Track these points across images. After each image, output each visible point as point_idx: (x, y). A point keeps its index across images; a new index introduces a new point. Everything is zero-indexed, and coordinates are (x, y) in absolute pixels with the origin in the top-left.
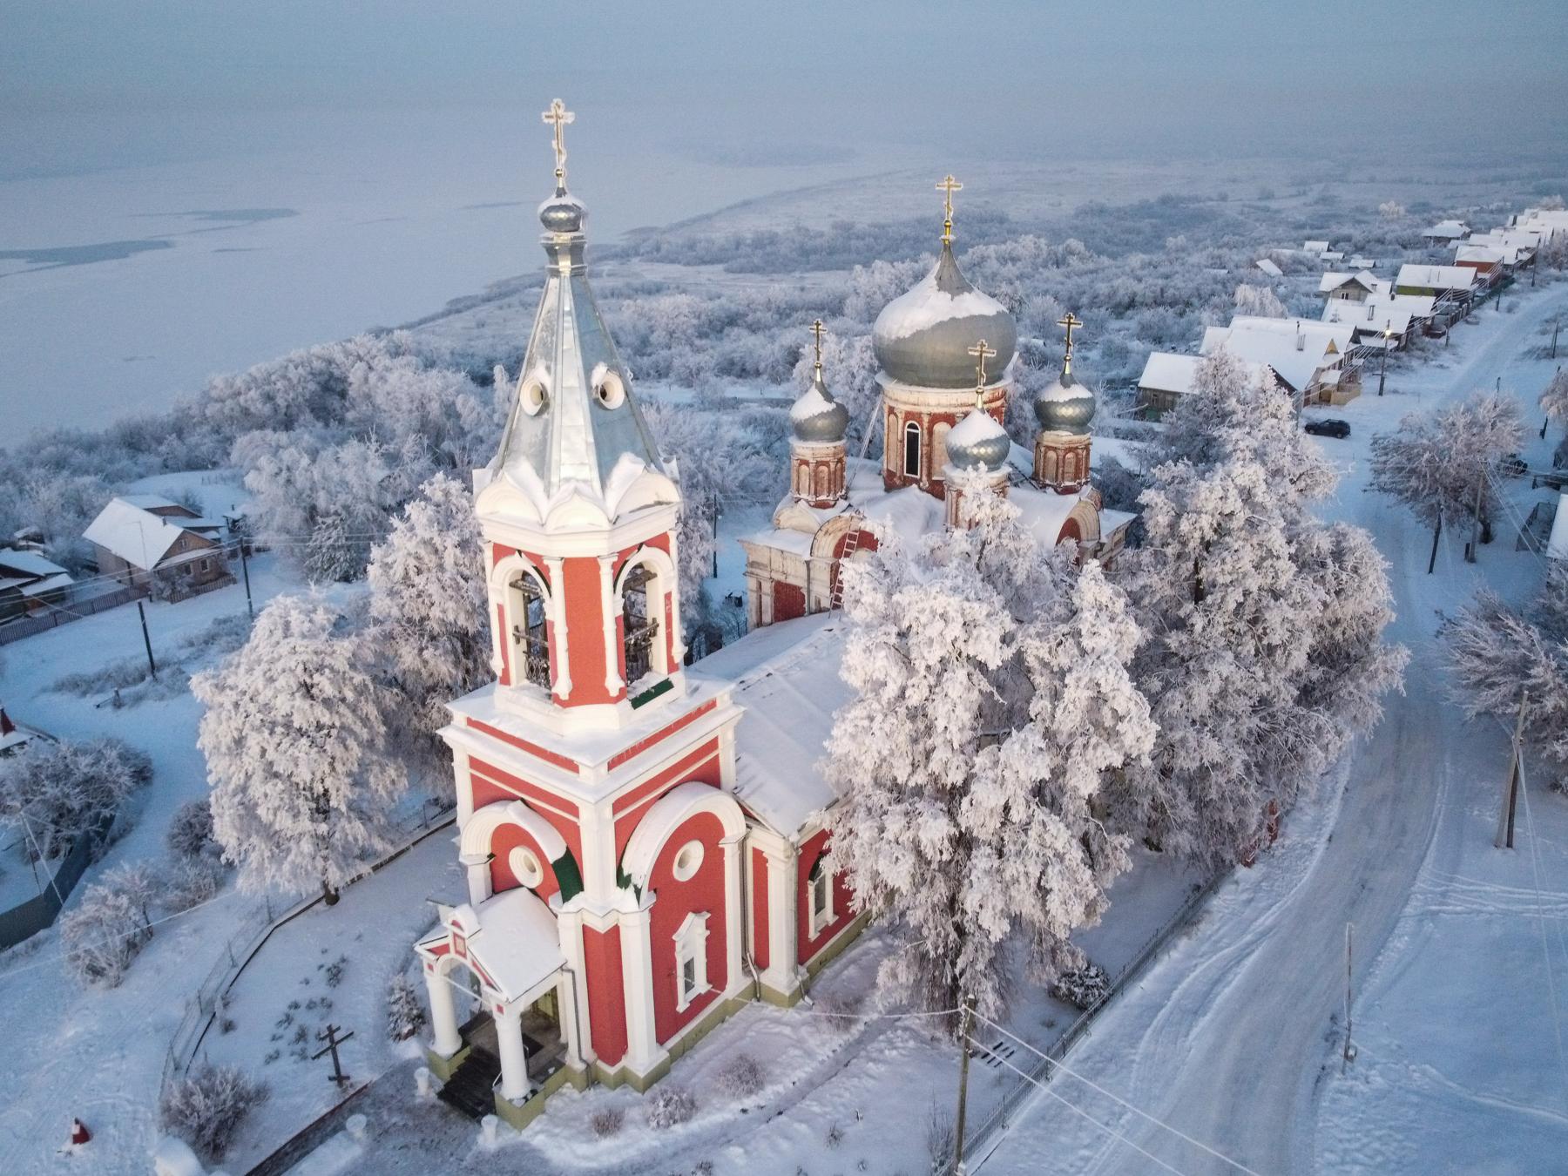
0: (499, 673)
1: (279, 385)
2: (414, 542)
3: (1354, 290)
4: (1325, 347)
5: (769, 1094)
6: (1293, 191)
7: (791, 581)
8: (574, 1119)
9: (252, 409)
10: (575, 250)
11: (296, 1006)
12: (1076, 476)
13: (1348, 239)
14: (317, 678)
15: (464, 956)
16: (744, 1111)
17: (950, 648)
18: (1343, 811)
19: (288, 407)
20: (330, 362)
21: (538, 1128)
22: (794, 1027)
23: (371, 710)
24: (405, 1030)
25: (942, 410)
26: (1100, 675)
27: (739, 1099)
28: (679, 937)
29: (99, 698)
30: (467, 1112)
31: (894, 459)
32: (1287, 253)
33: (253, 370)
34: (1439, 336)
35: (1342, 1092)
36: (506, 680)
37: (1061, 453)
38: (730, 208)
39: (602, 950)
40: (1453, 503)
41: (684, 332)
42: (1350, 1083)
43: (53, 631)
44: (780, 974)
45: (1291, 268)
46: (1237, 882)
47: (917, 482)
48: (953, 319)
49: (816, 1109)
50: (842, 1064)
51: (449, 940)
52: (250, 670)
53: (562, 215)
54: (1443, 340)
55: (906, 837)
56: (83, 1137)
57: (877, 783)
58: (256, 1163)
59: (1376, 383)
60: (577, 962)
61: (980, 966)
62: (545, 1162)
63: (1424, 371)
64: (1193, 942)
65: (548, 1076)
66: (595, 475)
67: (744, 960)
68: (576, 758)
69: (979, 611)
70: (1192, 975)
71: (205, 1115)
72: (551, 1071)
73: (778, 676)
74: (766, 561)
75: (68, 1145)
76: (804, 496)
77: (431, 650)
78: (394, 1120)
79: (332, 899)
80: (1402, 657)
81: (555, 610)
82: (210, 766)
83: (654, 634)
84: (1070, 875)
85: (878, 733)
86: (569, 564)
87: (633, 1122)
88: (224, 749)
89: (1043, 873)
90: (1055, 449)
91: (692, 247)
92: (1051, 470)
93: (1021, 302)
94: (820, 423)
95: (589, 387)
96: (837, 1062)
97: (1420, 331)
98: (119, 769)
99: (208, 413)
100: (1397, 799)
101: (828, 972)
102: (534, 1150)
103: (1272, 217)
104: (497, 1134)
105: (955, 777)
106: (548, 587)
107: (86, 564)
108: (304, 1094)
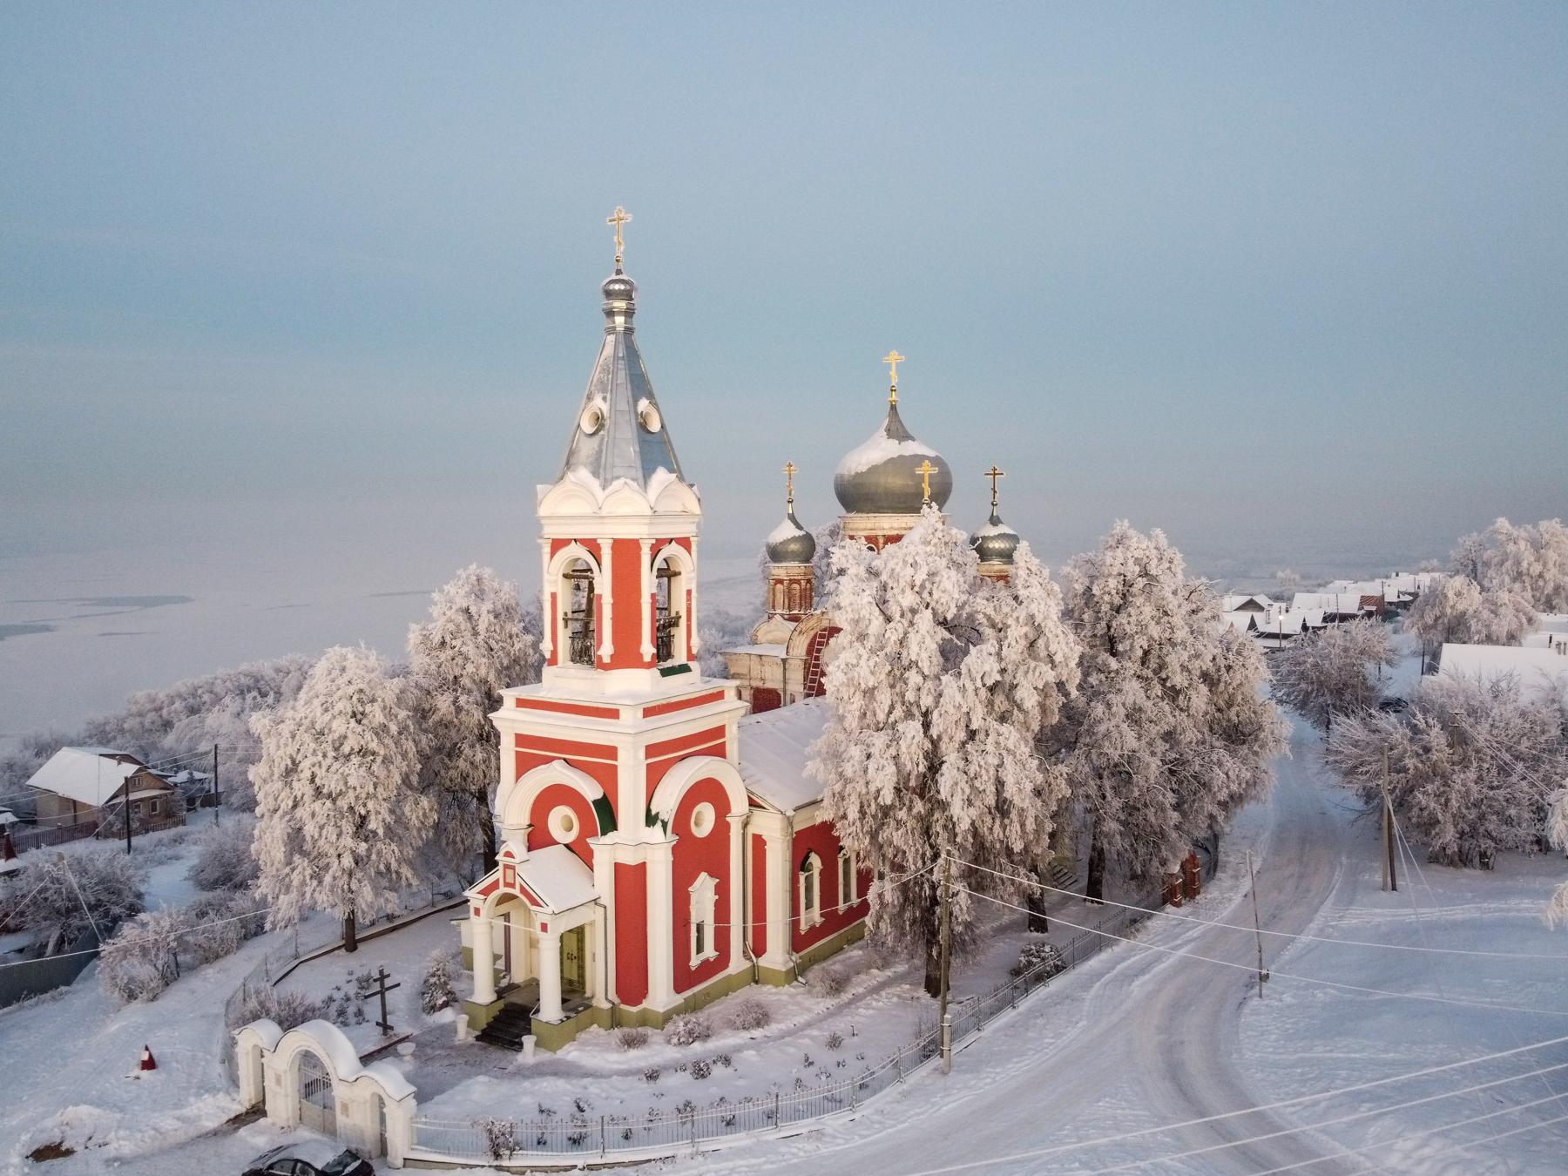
0: (548, 655)
5: (773, 1029)
7: (769, 685)
10: (629, 313)
14: (368, 708)
23: (409, 746)
25: (894, 533)
39: (630, 881)
44: (777, 955)
48: (901, 457)
50: (830, 1014)
56: (150, 1064)
74: (745, 671)
75: (137, 1072)
81: (604, 584)
86: (618, 545)
94: (793, 547)
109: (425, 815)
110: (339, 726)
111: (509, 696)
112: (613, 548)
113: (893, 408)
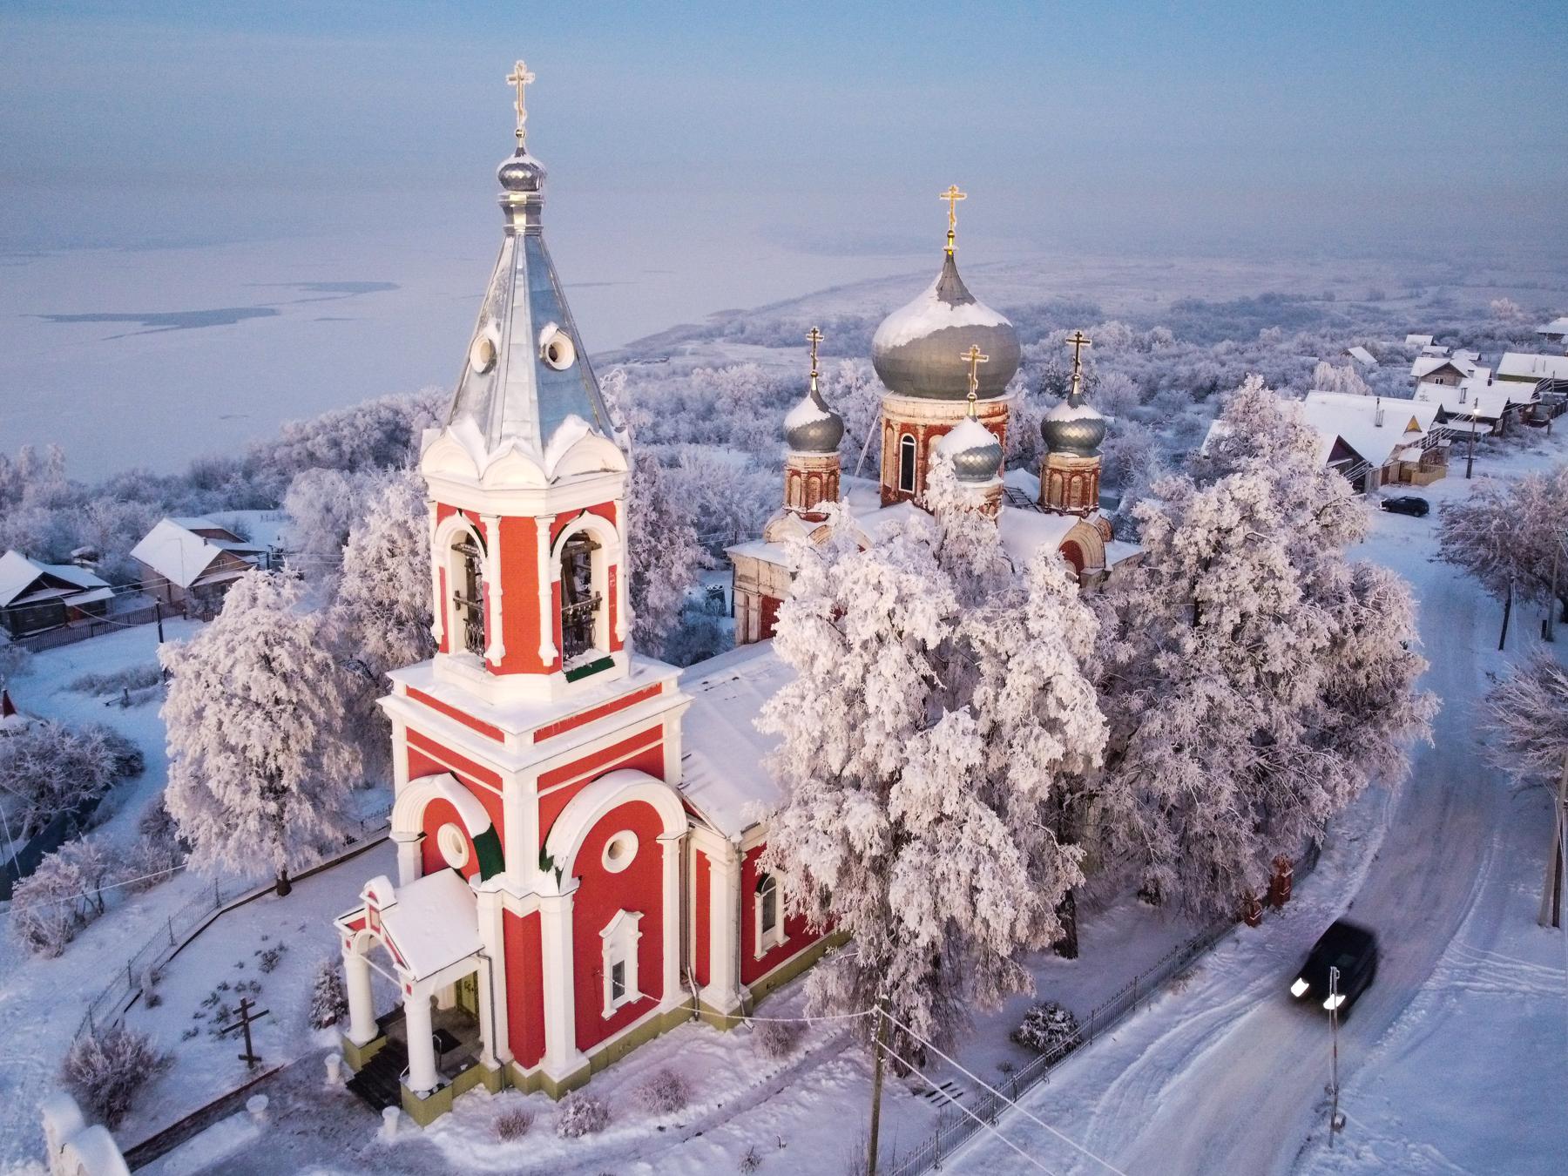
0: (439, 641)
1: (346, 432)
2: (389, 522)
3: (1448, 374)
4: (1406, 423)
5: (690, 1114)
6: (1405, 292)
8: (480, 1120)
9: (318, 454)
10: (532, 209)
11: (225, 987)
12: (1083, 502)
13: (1454, 333)
14: (277, 650)
15: (378, 930)
16: (661, 1129)
17: (888, 625)
18: (1371, 877)
19: (353, 453)
20: (397, 413)
21: (442, 1125)
22: (729, 1049)
23: (329, 689)
24: (326, 1018)
25: (938, 423)
26: (1041, 657)
27: (657, 1114)
28: (608, 934)
29: (109, 698)
30: (372, 1103)
31: (890, 475)
32: (1384, 345)
33: (323, 417)
34: (1542, 425)
35: (1327, 1166)
36: (444, 648)
37: (1067, 476)
38: (817, 294)
39: (522, 935)
40: (1526, 575)
41: (749, 400)
42: (1337, 1156)
43: (88, 641)
44: (720, 992)
45: (1385, 359)
46: (1237, 941)
47: (912, 497)
48: (951, 328)
49: (738, 1133)
50: (773, 1091)
51: (365, 914)
52: (214, 639)
53: (520, 174)
54: (1545, 429)
55: (836, 826)
57: (814, 773)
58: (151, 1135)
59: (1464, 466)
60: (495, 949)
61: (912, 978)
62: (442, 1160)
63: (1520, 456)
64: (1179, 998)
65: (460, 1073)
66: (537, 433)
67: (683, 974)
68: (501, 726)
69: (916, 584)
70: (1174, 1031)
71: (102, 1074)
72: (463, 1067)
73: (745, 681)
74: (754, 575)
76: (795, 508)
77: (395, 631)
78: (298, 1105)
79: (284, 887)
80: (1430, 706)
81: (491, 569)
82: (169, 736)
83: (597, 608)
84: (1003, 875)
85: (808, 712)
86: (507, 523)
87: (541, 1128)
88: (183, 719)
89: (974, 872)
90: (1060, 472)
91: (776, 328)
92: (1057, 492)
93: (1096, 381)
94: (812, 433)
95: (537, 347)
96: (770, 1088)
97: (1519, 418)
98: (103, 754)
99: (276, 455)
100: (1433, 871)
101: (775, 997)
102: (434, 1147)
103: (1376, 315)
104: (399, 1127)
105: (886, 766)
106: (485, 546)
107: (129, 580)
108: (214, 1069)
109: (347, 766)
110: (241, 675)
111: (400, 679)
112: (501, 527)
113: (950, 259)
